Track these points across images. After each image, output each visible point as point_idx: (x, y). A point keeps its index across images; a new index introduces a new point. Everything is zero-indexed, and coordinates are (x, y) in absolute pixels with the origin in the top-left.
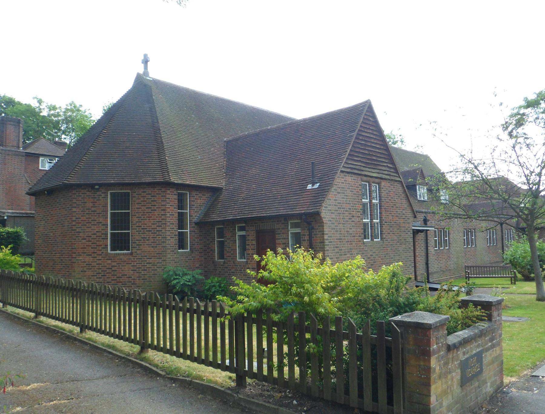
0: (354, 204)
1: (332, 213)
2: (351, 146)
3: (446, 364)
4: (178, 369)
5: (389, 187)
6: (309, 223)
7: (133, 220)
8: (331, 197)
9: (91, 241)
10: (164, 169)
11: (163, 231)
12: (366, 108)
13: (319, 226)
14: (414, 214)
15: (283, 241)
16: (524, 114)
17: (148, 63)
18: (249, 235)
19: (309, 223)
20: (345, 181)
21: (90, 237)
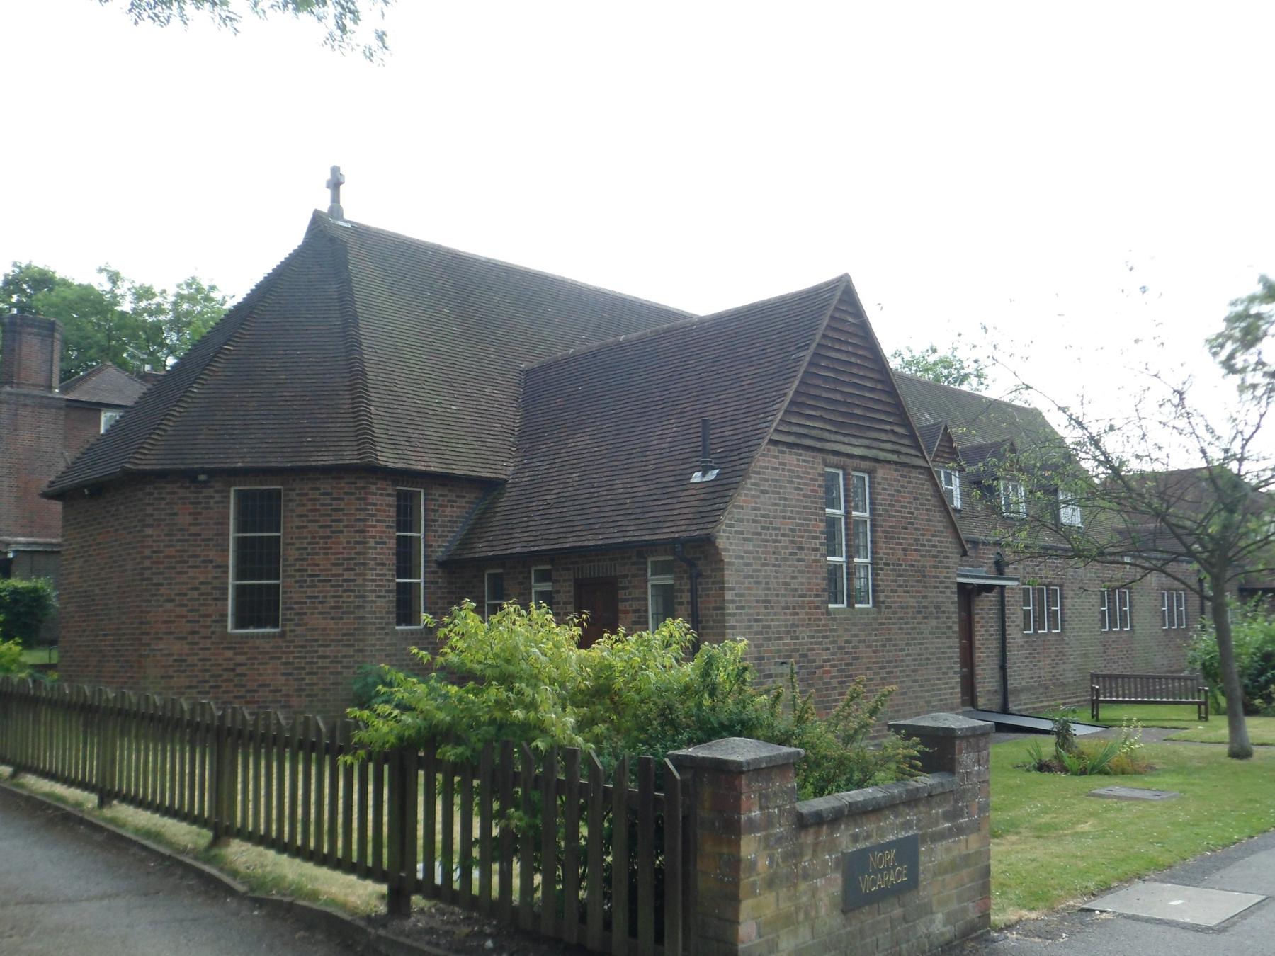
0: (805, 519)
1: (745, 539)
2: (796, 383)
3: (794, 855)
4: (278, 881)
5: (898, 481)
6: (691, 563)
7: (289, 554)
8: (745, 501)
9: (186, 606)
10: (364, 437)
11: (360, 581)
12: (838, 294)
13: (713, 570)
14: (962, 546)
15: (636, 605)
16: (1259, 316)
17: (342, 187)
18: (558, 592)
19: (691, 563)
20: (780, 464)
21: (185, 595)
